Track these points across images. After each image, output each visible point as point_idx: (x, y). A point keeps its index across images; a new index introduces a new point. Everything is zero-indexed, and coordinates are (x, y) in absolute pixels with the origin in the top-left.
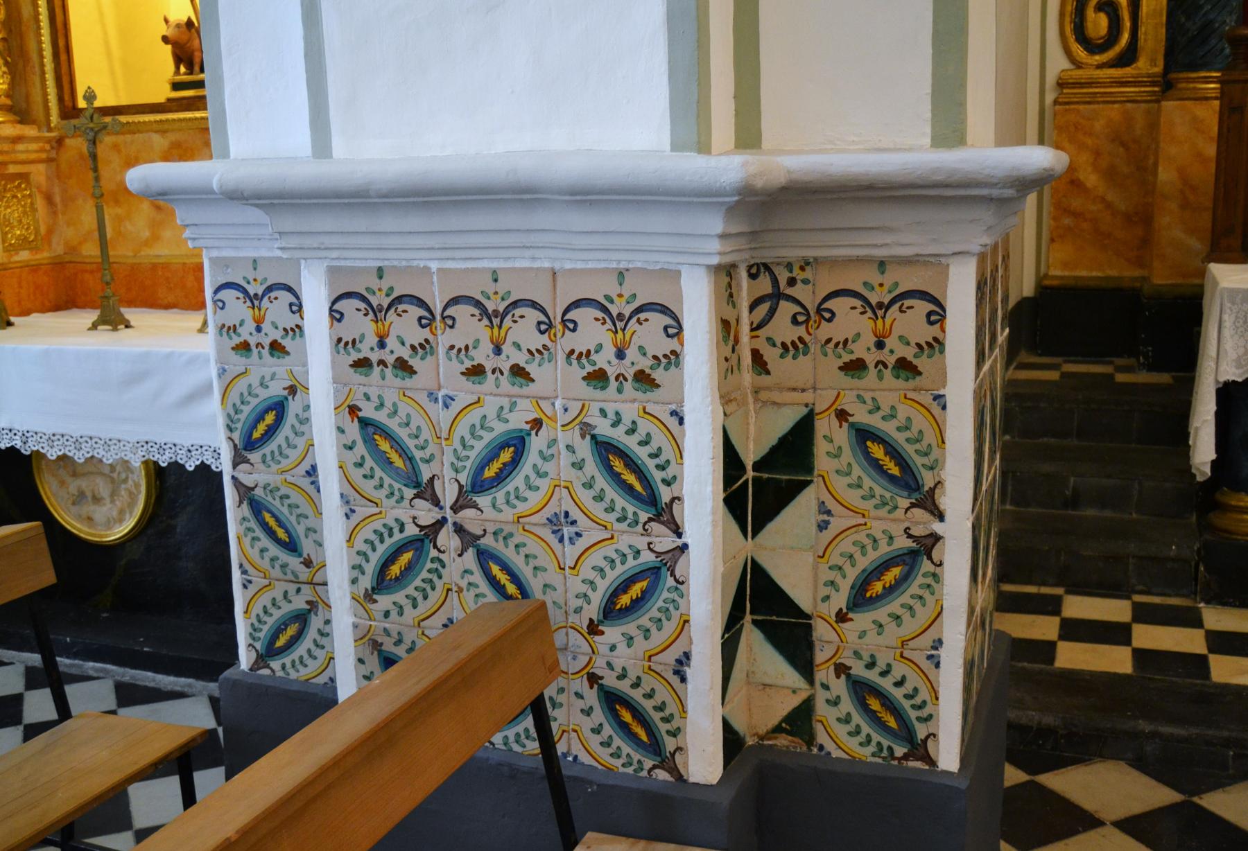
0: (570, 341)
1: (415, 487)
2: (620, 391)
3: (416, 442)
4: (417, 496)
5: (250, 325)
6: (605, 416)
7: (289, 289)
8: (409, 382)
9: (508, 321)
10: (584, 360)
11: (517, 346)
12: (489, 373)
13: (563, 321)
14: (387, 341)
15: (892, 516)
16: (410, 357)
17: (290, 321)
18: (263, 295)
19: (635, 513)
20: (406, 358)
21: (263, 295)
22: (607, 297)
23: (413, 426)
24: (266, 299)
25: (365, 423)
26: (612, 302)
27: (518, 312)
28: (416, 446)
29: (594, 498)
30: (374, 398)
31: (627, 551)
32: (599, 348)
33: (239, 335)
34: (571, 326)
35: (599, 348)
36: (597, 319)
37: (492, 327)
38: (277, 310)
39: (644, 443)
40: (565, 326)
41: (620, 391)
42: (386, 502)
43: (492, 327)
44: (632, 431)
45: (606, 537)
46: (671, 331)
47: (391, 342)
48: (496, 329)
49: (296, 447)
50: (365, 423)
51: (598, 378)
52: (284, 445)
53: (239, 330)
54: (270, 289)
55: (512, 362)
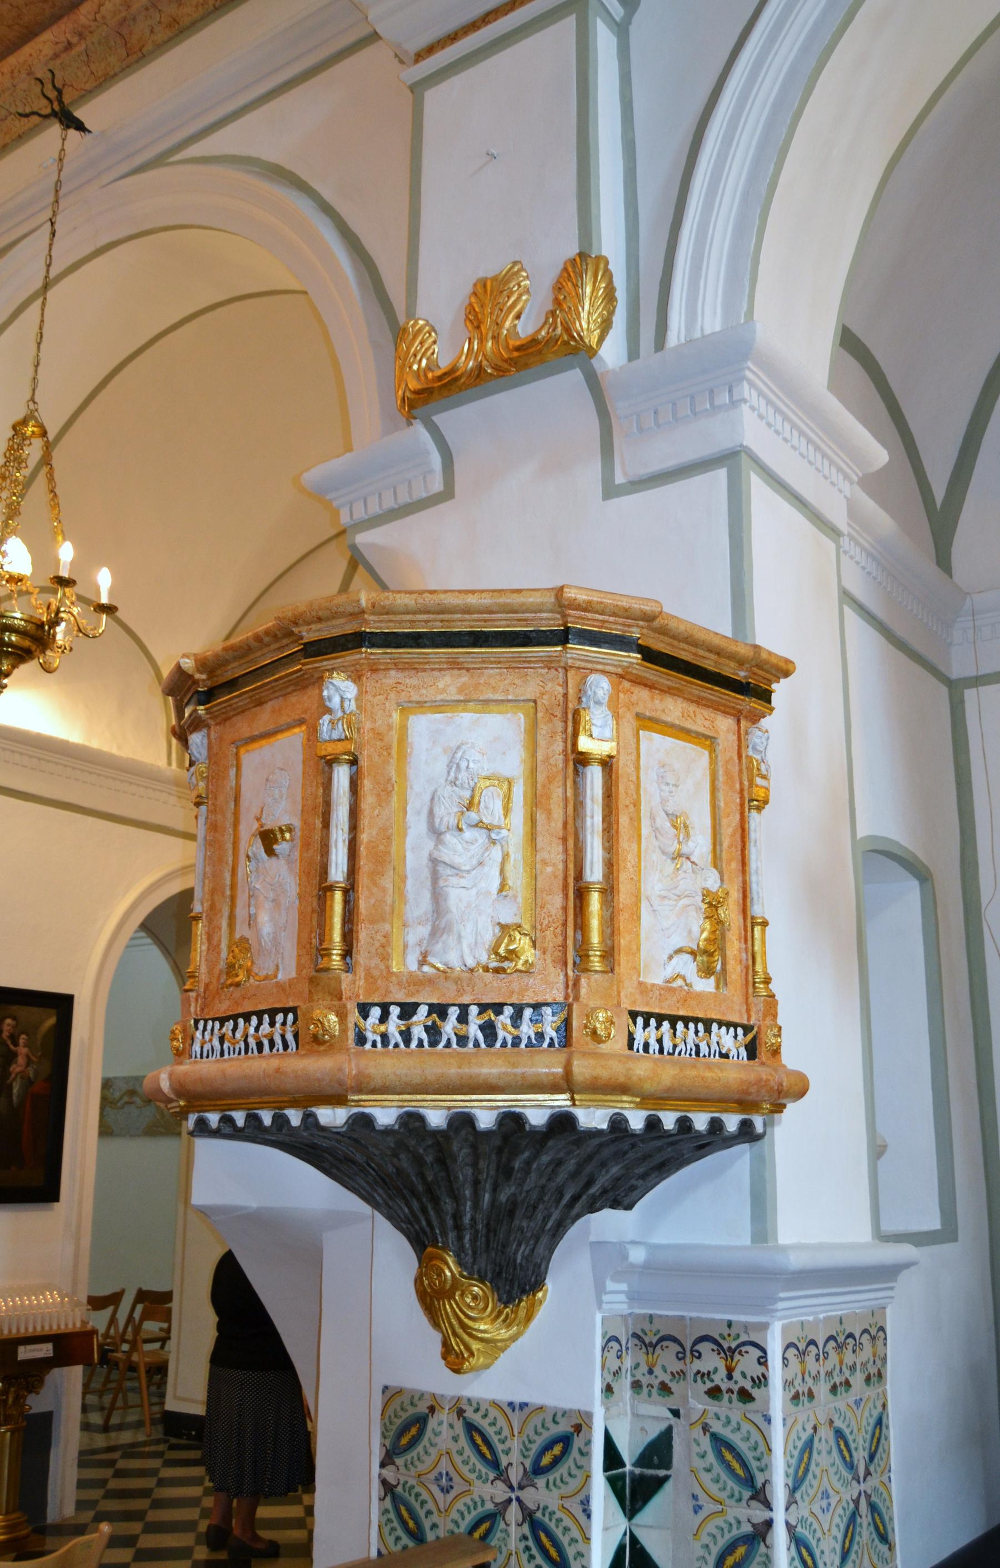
0: (698, 1365)
1: (519, 1484)
2: (650, 1395)
3: (754, 1454)
4: (752, 1498)
5: (723, 1372)
6: (719, 1419)
7: (675, 1340)
8: (750, 1406)
9: (737, 1357)
10: (706, 1378)
11: (744, 1375)
12: (645, 1387)
13: (692, 1351)
14: (655, 1369)
15: (819, 1476)
16: (671, 1381)
17: (758, 1370)
18: (657, 1343)
19: (740, 1492)
20: (667, 1381)
21: (657, 1343)
22: (721, 1335)
23: (752, 1441)
24: (659, 1347)
25: (715, 1438)
26: (646, 1334)
27: (665, 1343)
28: (754, 1458)
29: (712, 1480)
30: (723, 1418)
31: (733, 1521)
32: (716, 1370)
33: (712, 1381)
34: (697, 1354)
35: (716, 1370)
36: (713, 1350)
37: (648, 1354)
38: (747, 1363)
39: (493, 1424)
40: (693, 1355)
41: (650, 1395)
42: (728, 1502)
43: (648, 1354)
44: (485, 1416)
45: (717, 1510)
46: (680, 1355)
47: (658, 1371)
48: (650, 1355)
49: (430, 1455)
50: (715, 1438)
51: (714, 1393)
52: (416, 1458)
53: (712, 1376)
54: (663, 1339)
55: (740, 1385)
